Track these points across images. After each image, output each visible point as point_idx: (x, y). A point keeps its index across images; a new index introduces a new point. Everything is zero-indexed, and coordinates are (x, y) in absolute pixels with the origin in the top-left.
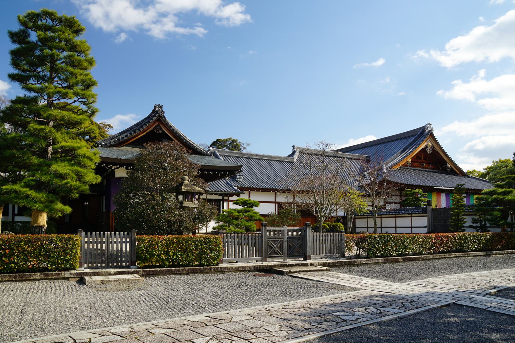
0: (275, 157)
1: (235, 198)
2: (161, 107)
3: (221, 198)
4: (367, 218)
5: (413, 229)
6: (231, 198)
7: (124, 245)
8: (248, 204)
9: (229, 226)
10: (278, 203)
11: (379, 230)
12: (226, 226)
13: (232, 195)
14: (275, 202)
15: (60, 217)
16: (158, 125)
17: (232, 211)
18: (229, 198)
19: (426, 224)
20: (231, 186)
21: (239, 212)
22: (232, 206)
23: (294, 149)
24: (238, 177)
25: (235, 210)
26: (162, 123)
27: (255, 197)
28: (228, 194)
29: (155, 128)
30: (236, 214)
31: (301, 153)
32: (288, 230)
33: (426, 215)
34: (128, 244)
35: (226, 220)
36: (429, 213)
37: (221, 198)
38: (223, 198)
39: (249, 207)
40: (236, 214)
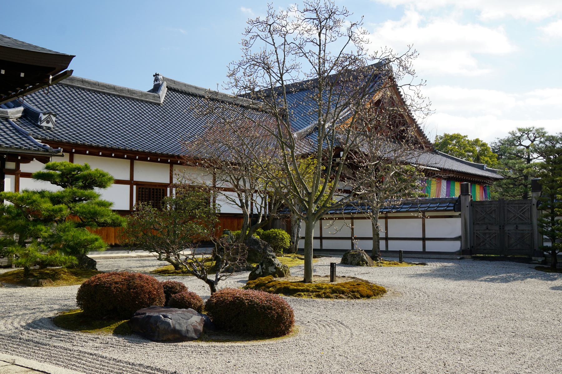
0: (122, 90)
1: (35, 167)
4: (352, 218)
6: (24, 168)
8: (77, 179)
9: (22, 244)
10: (138, 184)
11: (382, 244)
12: (12, 243)
13: (27, 159)
14: (131, 182)
17: (36, 197)
18: (18, 167)
19: (458, 232)
20: (26, 135)
21: (55, 199)
22: (27, 184)
23: (156, 80)
24: (43, 117)
25: (42, 194)
27: (96, 165)
28: (17, 155)
30: (47, 205)
31: (169, 89)
33: (457, 214)
34: (135, 187)
35: (12, 224)
36: (466, 211)
39: (85, 187)
40: (47, 205)
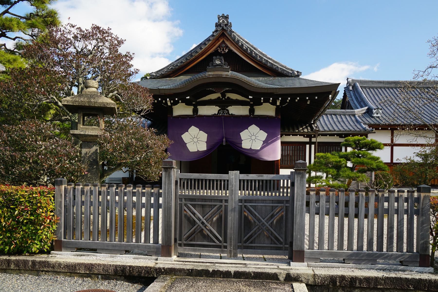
2: (227, 17)
3: (307, 140)
5: (395, 148)
7: (285, 185)
15: (154, 128)
16: (223, 42)
26: (228, 40)
29: (219, 46)
32: (226, 188)
34: (282, 185)
37: (307, 140)
38: (310, 140)
